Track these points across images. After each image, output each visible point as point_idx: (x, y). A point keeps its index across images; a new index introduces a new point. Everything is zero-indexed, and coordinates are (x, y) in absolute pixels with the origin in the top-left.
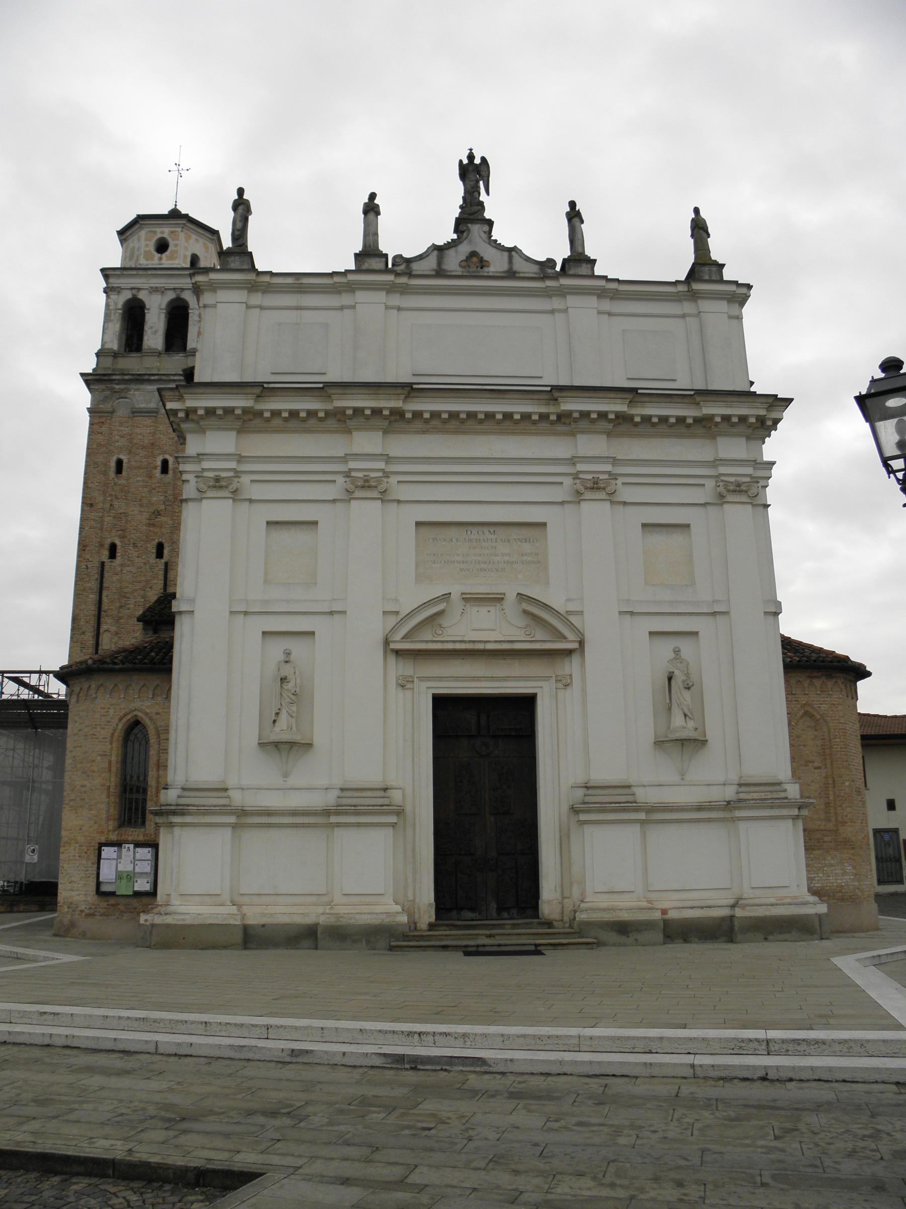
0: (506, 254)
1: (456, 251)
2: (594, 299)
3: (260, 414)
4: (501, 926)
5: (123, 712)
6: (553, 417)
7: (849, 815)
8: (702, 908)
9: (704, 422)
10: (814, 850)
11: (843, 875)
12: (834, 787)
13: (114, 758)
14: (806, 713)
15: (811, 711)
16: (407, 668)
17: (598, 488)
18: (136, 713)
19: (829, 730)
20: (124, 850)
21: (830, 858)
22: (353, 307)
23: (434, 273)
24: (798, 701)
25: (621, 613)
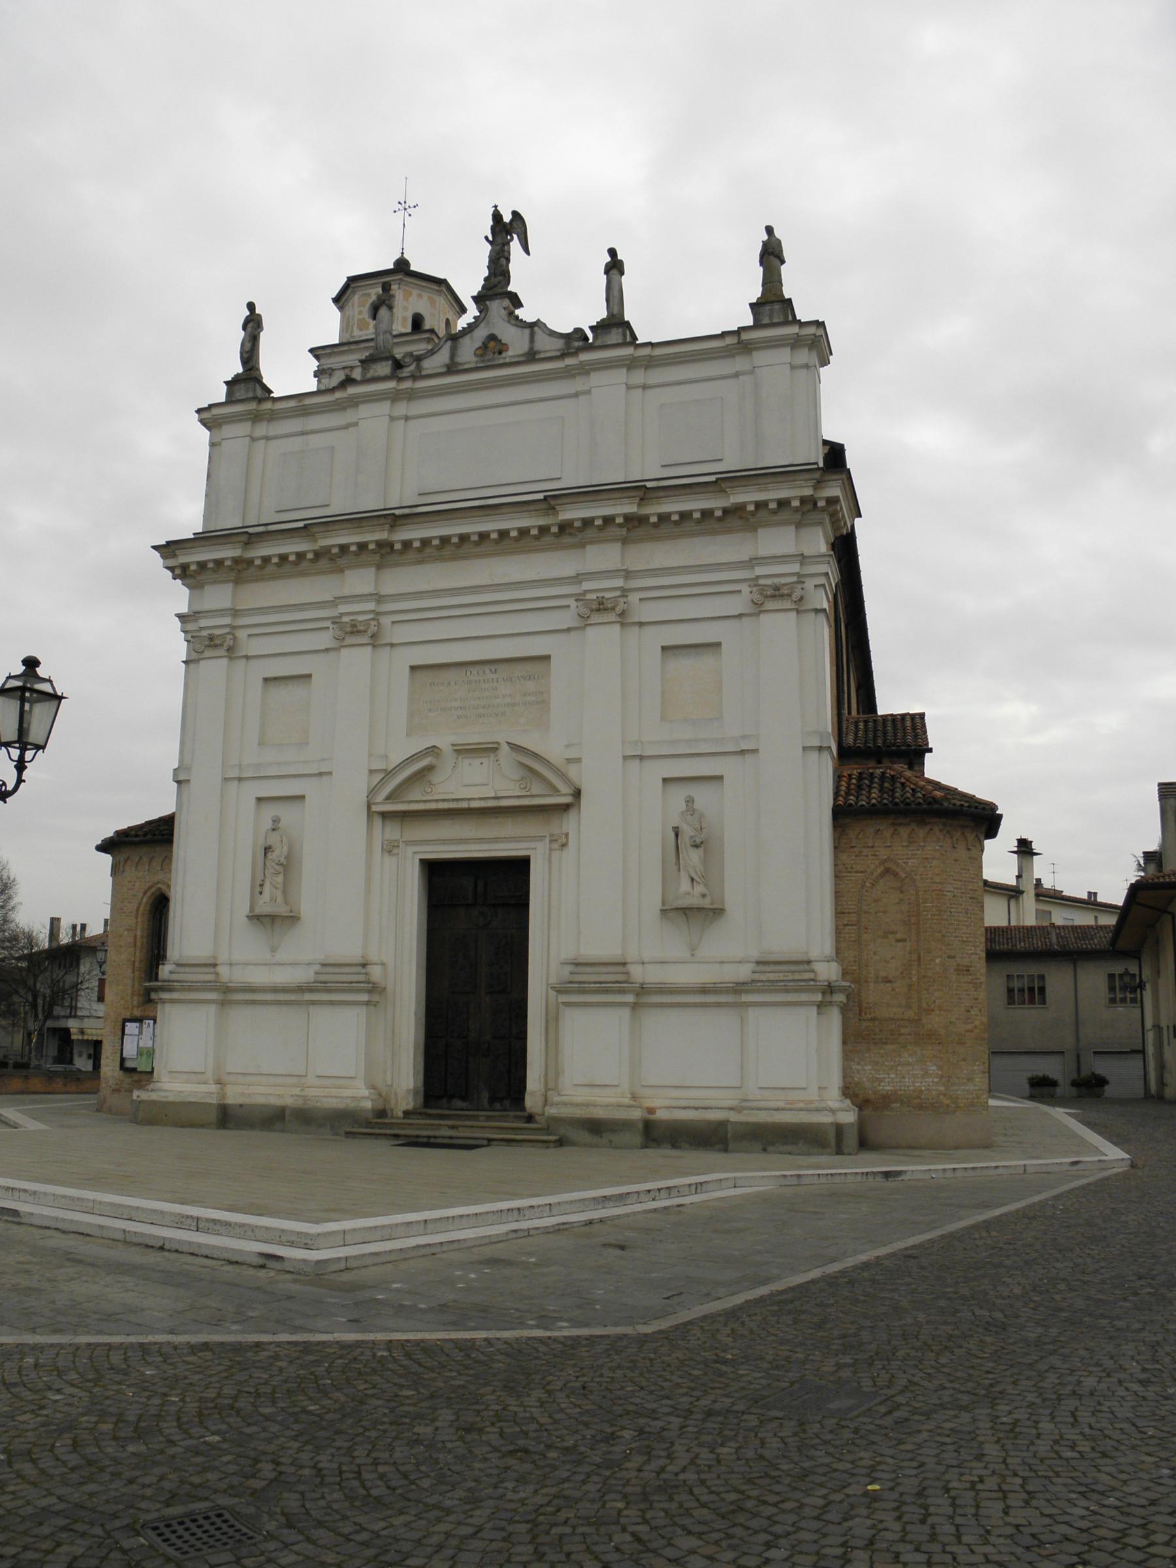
0: (527, 331)
1: (472, 338)
2: (787, 351)
3: (250, 562)
4: (475, 1118)
5: (148, 885)
6: (555, 529)
7: (937, 1001)
8: (696, 1108)
9: (734, 512)
10: (886, 1043)
11: (923, 1077)
12: (919, 965)
13: (139, 933)
14: (887, 871)
15: (894, 868)
16: (393, 832)
17: (606, 609)
18: (160, 886)
19: (917, 893)
20: (145, 1026)
21: (906, 1055)
22: (588, 392)
23: (444, 370)
24: (876, 855)
25: (805, 749)
